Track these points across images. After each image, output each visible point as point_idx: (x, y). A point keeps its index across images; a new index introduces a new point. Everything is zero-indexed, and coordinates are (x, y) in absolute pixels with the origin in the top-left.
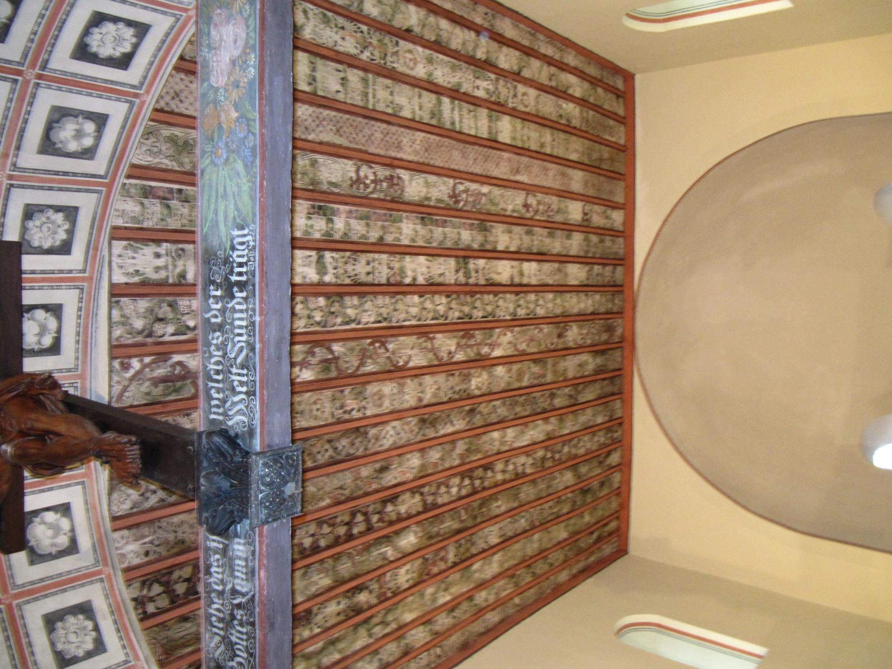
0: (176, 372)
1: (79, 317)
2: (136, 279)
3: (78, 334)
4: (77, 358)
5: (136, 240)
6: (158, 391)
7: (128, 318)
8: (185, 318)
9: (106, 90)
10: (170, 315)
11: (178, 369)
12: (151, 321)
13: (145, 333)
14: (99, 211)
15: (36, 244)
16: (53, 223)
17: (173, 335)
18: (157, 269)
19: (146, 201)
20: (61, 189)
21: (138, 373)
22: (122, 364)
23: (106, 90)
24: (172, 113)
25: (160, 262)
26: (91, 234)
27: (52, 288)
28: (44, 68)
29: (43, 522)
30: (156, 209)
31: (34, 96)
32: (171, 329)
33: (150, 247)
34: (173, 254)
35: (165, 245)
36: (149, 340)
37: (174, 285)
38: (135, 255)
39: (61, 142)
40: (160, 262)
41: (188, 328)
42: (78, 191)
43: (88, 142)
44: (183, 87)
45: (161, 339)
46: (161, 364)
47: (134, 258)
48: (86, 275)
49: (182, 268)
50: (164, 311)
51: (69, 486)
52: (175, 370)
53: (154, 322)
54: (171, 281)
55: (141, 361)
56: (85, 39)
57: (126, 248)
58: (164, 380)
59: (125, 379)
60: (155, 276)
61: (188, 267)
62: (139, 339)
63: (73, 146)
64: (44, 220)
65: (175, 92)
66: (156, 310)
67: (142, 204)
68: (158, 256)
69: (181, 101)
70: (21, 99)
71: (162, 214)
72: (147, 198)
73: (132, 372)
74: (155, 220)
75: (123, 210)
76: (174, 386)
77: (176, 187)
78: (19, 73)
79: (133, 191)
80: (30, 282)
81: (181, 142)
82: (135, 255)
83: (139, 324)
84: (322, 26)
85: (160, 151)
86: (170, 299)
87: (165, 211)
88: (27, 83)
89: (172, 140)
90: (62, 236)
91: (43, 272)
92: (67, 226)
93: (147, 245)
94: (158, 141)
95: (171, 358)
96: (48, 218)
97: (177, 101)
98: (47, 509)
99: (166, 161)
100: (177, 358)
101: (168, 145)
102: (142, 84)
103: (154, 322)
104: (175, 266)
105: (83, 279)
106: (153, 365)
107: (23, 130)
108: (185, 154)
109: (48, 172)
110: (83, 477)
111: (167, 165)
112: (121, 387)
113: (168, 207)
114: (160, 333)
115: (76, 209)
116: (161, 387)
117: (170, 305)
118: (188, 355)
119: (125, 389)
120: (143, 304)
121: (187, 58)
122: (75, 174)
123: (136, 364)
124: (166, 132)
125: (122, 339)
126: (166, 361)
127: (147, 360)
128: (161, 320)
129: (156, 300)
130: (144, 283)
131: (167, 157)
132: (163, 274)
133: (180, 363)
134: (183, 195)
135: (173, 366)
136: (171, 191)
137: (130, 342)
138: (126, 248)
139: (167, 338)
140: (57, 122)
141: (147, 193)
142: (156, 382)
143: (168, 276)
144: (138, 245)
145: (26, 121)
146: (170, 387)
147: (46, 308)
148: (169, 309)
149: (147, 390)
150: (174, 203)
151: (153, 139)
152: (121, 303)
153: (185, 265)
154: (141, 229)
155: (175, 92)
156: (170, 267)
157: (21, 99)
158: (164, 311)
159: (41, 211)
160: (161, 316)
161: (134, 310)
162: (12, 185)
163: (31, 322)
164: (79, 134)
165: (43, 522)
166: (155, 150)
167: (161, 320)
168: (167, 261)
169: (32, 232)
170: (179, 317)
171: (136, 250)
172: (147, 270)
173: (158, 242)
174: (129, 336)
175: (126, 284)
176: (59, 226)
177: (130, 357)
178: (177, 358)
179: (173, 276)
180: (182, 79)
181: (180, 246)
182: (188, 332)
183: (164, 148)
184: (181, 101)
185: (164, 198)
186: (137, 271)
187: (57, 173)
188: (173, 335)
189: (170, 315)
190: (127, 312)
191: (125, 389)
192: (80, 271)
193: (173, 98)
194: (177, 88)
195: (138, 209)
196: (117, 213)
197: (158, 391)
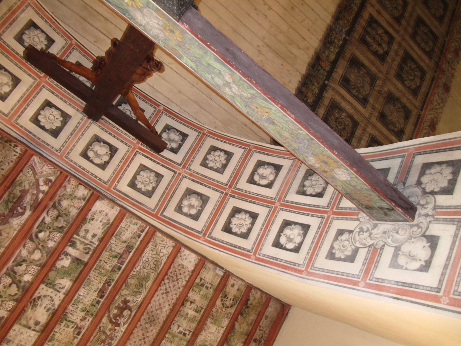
0: (19, 208)
1: (92, 174)
2: (89, 217)
3: (84, 169)
4: (72, 161)
5: (109, 228)
6: (17, 191)
7: (72, 200)
8: (48, 233)
9: (212, 221)
10: (56, 224)
11: (20, 210)
12: (61, 211)
13: (57, 205)
14: (144, 207)
15: (142, 173)
16: (148, 184)
17: (44, 218)
18: (87, 231)
19: (125, 245)
20: (164, 193)
21: (38, 185)
22: (50, 181)
23: (212, 221)
24: (160, 285)
25: (89, 236)
26: (133, 199)
27: (115, 170)
28: (231, 196)
29: (7, 84)
30: (118, 249)
31: (217, 191)
32: (48, 220)
33: (100, 234)
34: (88, 246)
35: (97, 243)
36: (51, 204)
37: (72, 237)
38: (102, 223)
39: (189, 198)
40: (89, 236)
41: (40, 231)
42: (159, 201)
43: (185, 210)
44: (169, 298)
45: (46, 211)
46: (32, 202)
47: (101, 222)
48: (112, 189)
49: (78, 247)
50: (61, 223)
51: (12, 109)
52: (21, 208)
53: (59, 213)
54: (75, 236)
55: (43, 192)
56: (243, 212)
57: (108, 220)
58: (21, 198)
59: (41, 178)
60: (84, 227)
61: (76, 251)
62: (57, 199)
63: (185, 203)
64: (152, 181)
65: (168, 292)
66: (65, 218)
67: (125, 242)
68: (94, 236)
69: (163, 294)
70: (217, 186)
71: (114, 251)
72: (127, 246)
73: (41, 183)
74: (113, 245)
75: (127, 230)
76: (11, 202)
77: (123, 267)
78: (230, 187)
79: (134, 240)
80: (124, 162)
81: (144, 282)
82: (102, 223)
83: (65, 203)
84: (377, 114)
85: (145, 267)
86: (65, 230)
87: (114, 254)
88: (225, 189)
89: (146, 278)
90: (139, 185)
91: (126, 170)
92: (143, 189)
93: (102, 233)
94: (150, 269)
95: (30, 210)
96: (152, 183)
97: (164, 291)
98: (11, 91)
99: (139, 268)
100: (28, 213)
101: (146, 274)
102: (211, 238)
103: (59, 213)
104: (82, 243)
105: (111, 186)
106: (35, 197)
107: (201, 184)
108: (137, 282)
109: (176, 189)
110: (10, 118)
111: (136, 268)
112: (37, 172)
113: (115, 257)
114: (50, 213)
115: (150, 197)
116: (18, 194)
117: (62, 227)
118: (23, 222)
119: (35, 173)
120: (74, 212)
121: (181, 309)
122: (169, 201)
123: (44, 188)
124: (153, 276)
125: (63, 190)
126: (31, 206)
127: (41, 196)
128: (57, 218)
129: (71, 221)
130: (84, 220)
131: (140, 270)
132: (82, 233)
133: (22, 214)
134: (116, 270)
135: (25, 209)
136: (122, 263)
137: (59, 193)
138: (108, 220)
139: (44, 214)
140: (201, 198)
141: (129, 248)
142: (24, 193)
143: (79, 236)
144: (105, 228)
145: (205, 186)
146: (13, 199)
147: (107, 163)
148: (60, 226)
149: (23, 185)
150: (116, 260)
151: (153, 266)
152: (82, 201)
153: (78, 249)
154: (113, 235)
155: (168, 292)
156: (83, 240)
157: (217, 186)
158: (61, 223)
159: (157, 181)
160: (60, 218)
161: (74, 205)
162: (176, 173)
163: (105, 153)
164: (191, 206)
165: (7, 84)
166: (147, 265)
167: (57, 218)
168: (87, 240)
169: (148, 174)
170: (51, 230)
171: (104, 224)
172: (90, 225)
173: (101, 240)
174: (62, 194)
175: (90, 210)
176: (145, 186)
177: (50, 187)
178: (28, 213)
179: (76, 239)
180: (173, 299)
181: (91, 253)
182: (37, 230)
183: (145, 270)
184: (163, 294)
185: (121, 257)
186: (93, 219)
187: (174, 193)
188: (44, 218)
189: (56, 224)
190: (76, 201)
191: (35, 173)
192: (115, 186)
193: (166, 289)
194: (169, 295)
195: (124, 238)
196: (127, 226)
197: (17, 191)
